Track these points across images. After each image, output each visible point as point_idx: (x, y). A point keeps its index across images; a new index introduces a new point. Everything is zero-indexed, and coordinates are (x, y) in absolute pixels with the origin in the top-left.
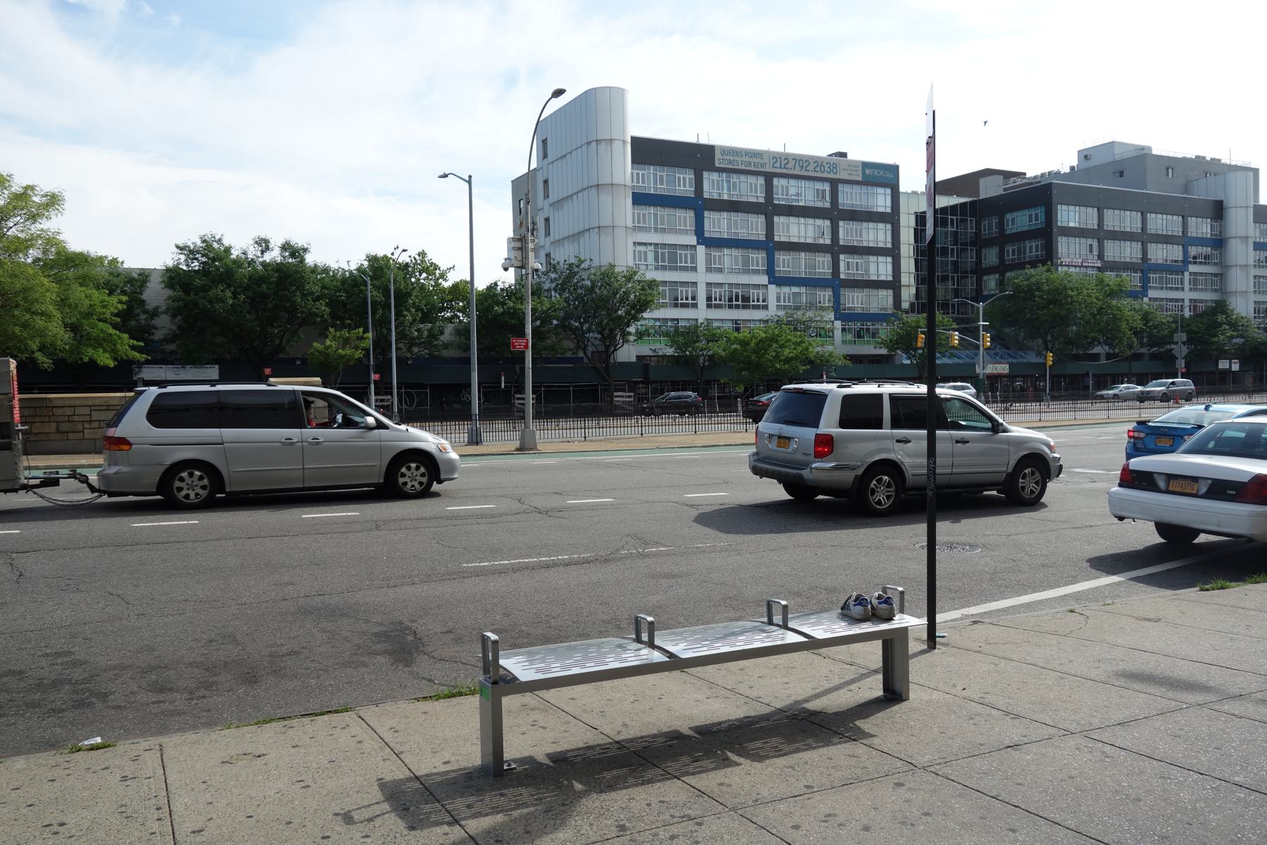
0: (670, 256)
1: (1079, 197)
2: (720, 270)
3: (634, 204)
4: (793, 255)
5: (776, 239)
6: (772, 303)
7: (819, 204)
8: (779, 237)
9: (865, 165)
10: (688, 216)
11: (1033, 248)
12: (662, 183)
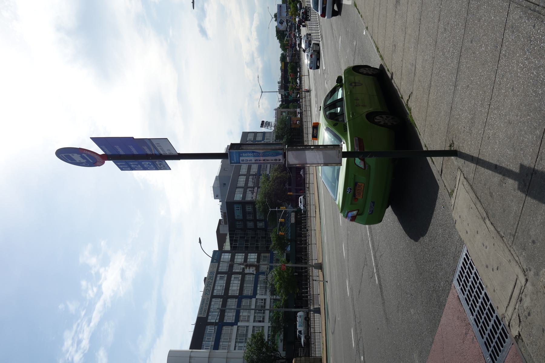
0: (241, 337)
1: (232, 193)
2: (249, 317)
3: (218, 349)
4: (245, 288)
5: (238, 295)
6: (263, 297)
7: (225, 279)
8: (237, 293)
10: (225, 329)
11: (249, 209)
12: (210, 339)
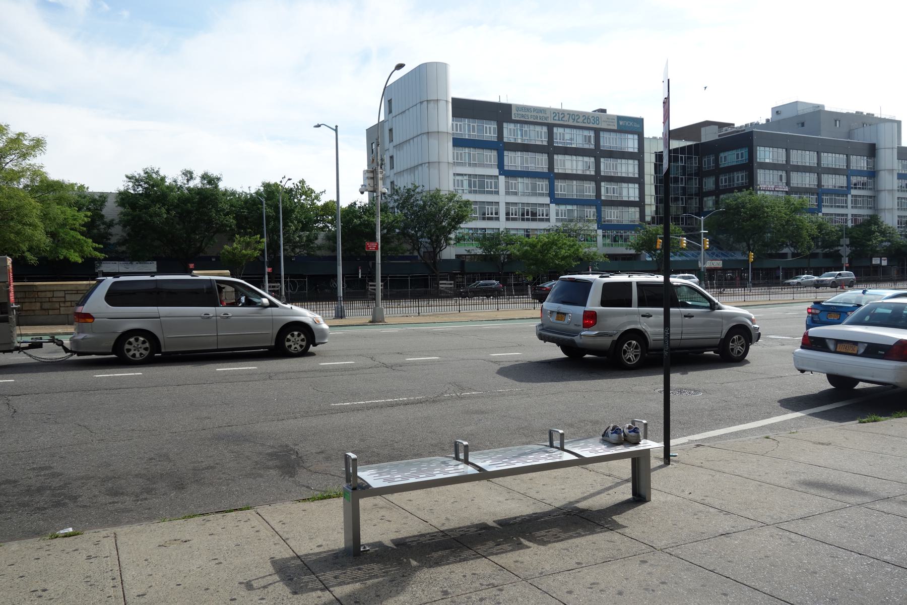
0: (479, 184)
1: (772, 141)
2: (516, 194)
3: (454, 146)
4: (568, 182)
5: (556, 171)
6: (553, 217)
7: (586, 146)
8: (558, 169)
9: (620, 118)
10: (492, 155)
11: (739, 178)
12: (474, 131)
